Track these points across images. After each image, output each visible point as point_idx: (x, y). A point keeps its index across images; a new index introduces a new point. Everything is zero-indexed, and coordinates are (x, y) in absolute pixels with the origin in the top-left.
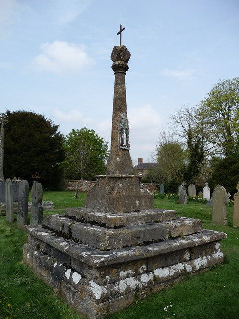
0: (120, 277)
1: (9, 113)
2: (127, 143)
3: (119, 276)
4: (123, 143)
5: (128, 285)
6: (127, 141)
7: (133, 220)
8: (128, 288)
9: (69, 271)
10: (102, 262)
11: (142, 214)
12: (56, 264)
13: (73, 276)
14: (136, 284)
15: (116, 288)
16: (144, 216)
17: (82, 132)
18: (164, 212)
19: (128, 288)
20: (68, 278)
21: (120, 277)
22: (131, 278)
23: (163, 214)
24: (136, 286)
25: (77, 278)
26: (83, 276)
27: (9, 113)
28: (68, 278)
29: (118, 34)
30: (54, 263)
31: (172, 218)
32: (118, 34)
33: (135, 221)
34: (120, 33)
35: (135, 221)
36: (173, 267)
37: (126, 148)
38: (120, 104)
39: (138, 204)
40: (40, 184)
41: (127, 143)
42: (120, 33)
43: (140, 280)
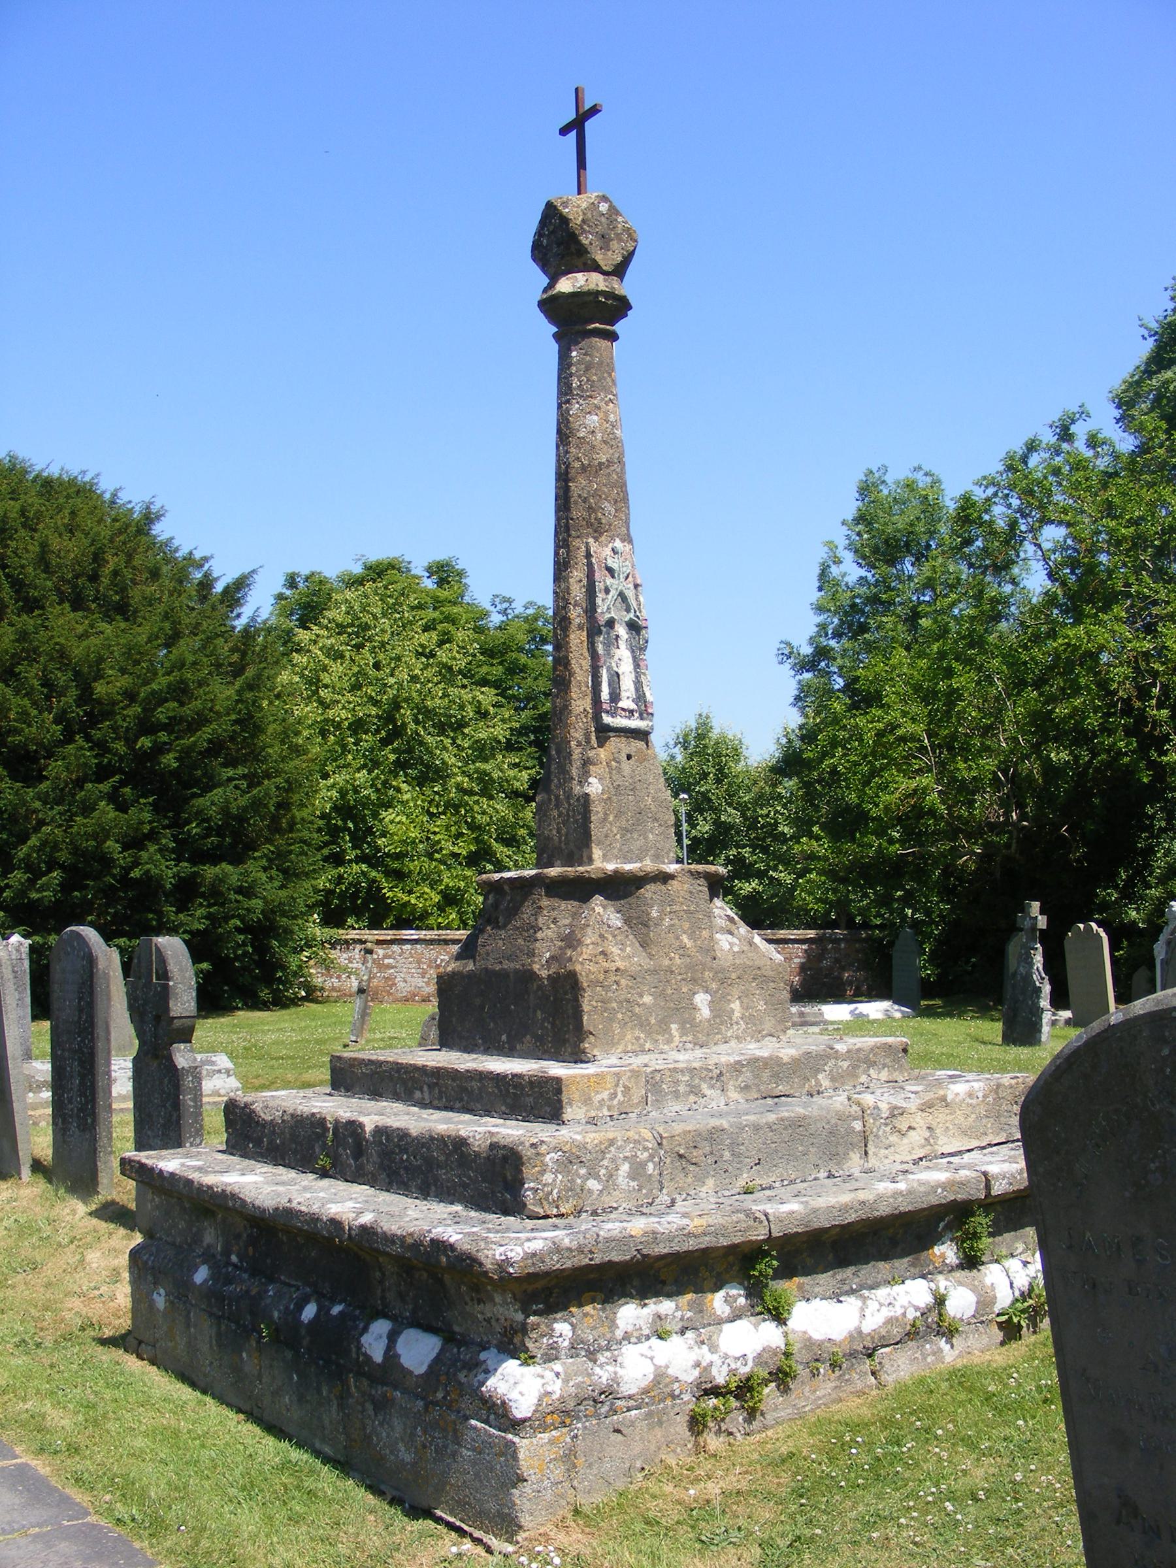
0: (619, 1334)
1: (150, 517)
2: (640, 698)
3: (613, 1325)
4: (615, 697)
5: (657, 1367)
6: (638, 685)
7: (682, 1088)
8: (660, 1377)
9: (381, 1327)
10: (534, 1255)
11: (725, 1054)
12: (309, 1312)
13: (400, 1347)
14: (697, 1364)
15: (603, 1374)
16: (737, 1068)
17: (471, 1266)
18: (841, 1047)
19: (660, 1377)
20: (378, 1357)
21: (619, 1334)
22: (676, 1339)
23: (837, 1056)
24: (696, 1372)
25: (418, 1351)
26: (450, 1338)
27: (150, 517)
28: (378, 1357)
29: (564, 131)
30: (300, 1308)
31: (884, 1075)
32: (564, 131)
33: (695, 1091)
34: (577, 125)
35: (695, 1091)
36: (882, 1293)
37: (635, 723)
38: (582, 503)
39: (706, 1012)
40: (134, 1183)
41: (640, 698)
42: (577, 125)
43: (713, 1349)
